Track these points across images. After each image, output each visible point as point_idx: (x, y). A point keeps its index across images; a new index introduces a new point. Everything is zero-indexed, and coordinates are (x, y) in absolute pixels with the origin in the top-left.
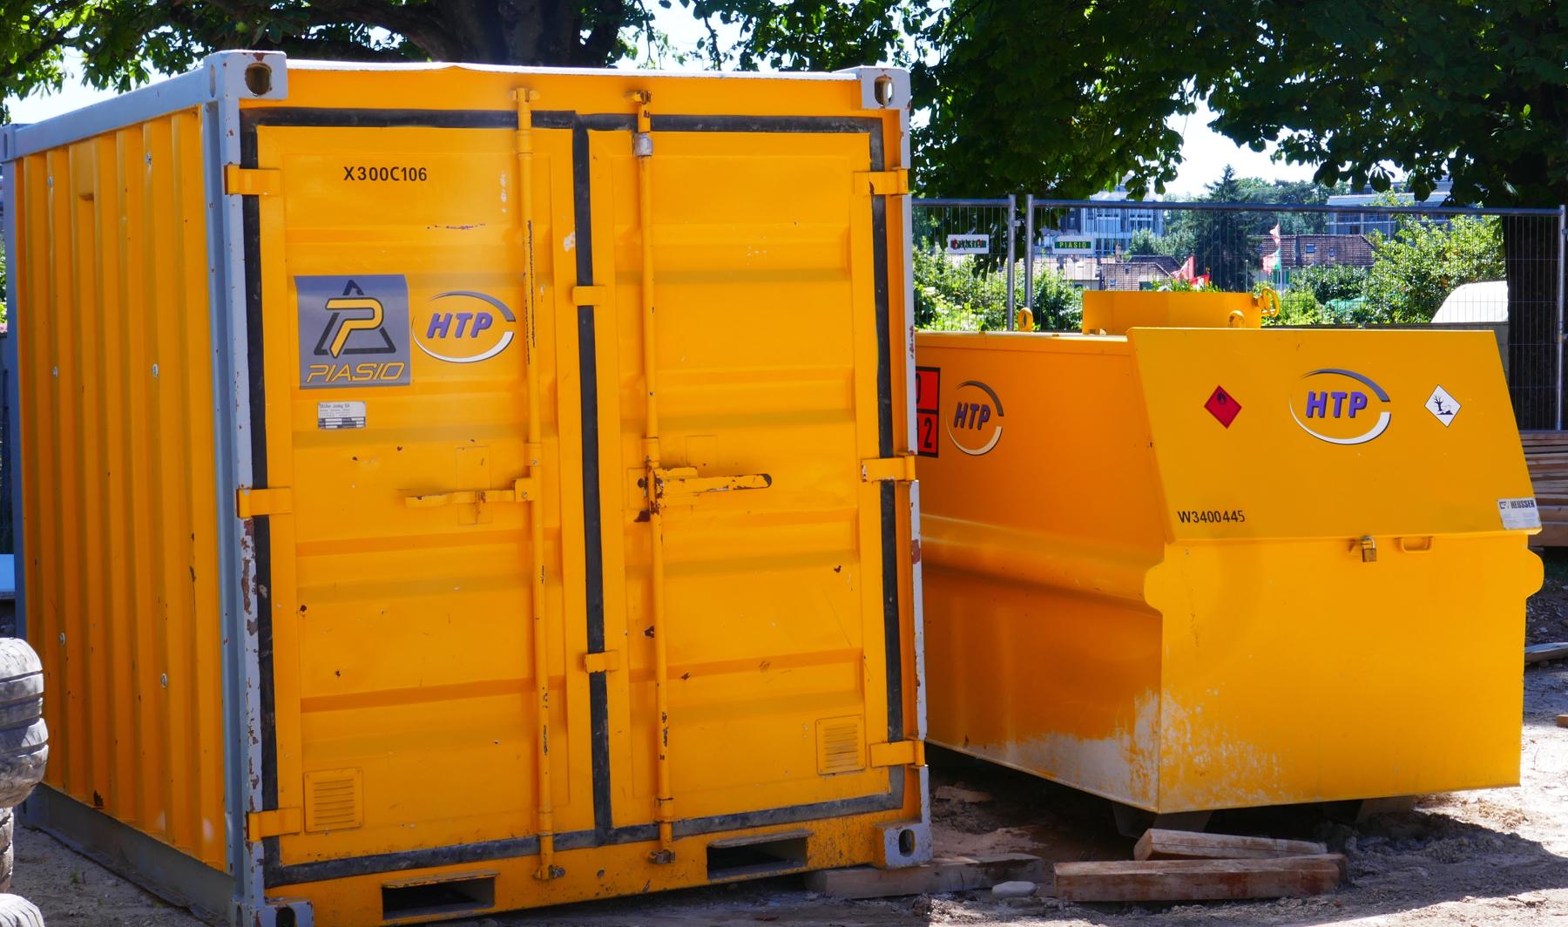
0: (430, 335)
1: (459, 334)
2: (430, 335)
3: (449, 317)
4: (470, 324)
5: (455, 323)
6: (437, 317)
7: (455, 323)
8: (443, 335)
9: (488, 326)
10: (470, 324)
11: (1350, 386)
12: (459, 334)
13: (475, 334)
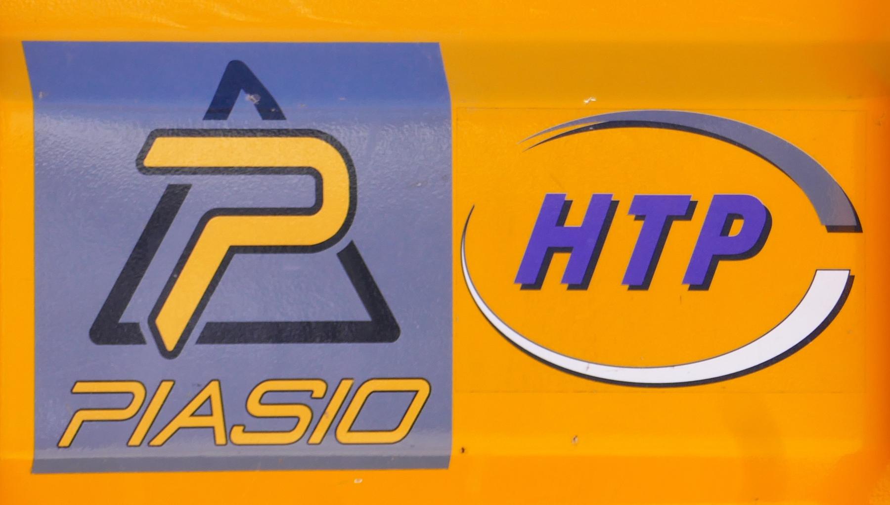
0: (532, 277)
1: (640, 276)
2: (532, 277)
3: (604, 210)
4: (683, 239)
5: (625, 233)
6: (557, 207)
7: (625, 233)
8: (580, 279)
9: (752, 246)
10: (683, 239)
11: (706, 172)
12: (640, 276)
13: (700, 278)
